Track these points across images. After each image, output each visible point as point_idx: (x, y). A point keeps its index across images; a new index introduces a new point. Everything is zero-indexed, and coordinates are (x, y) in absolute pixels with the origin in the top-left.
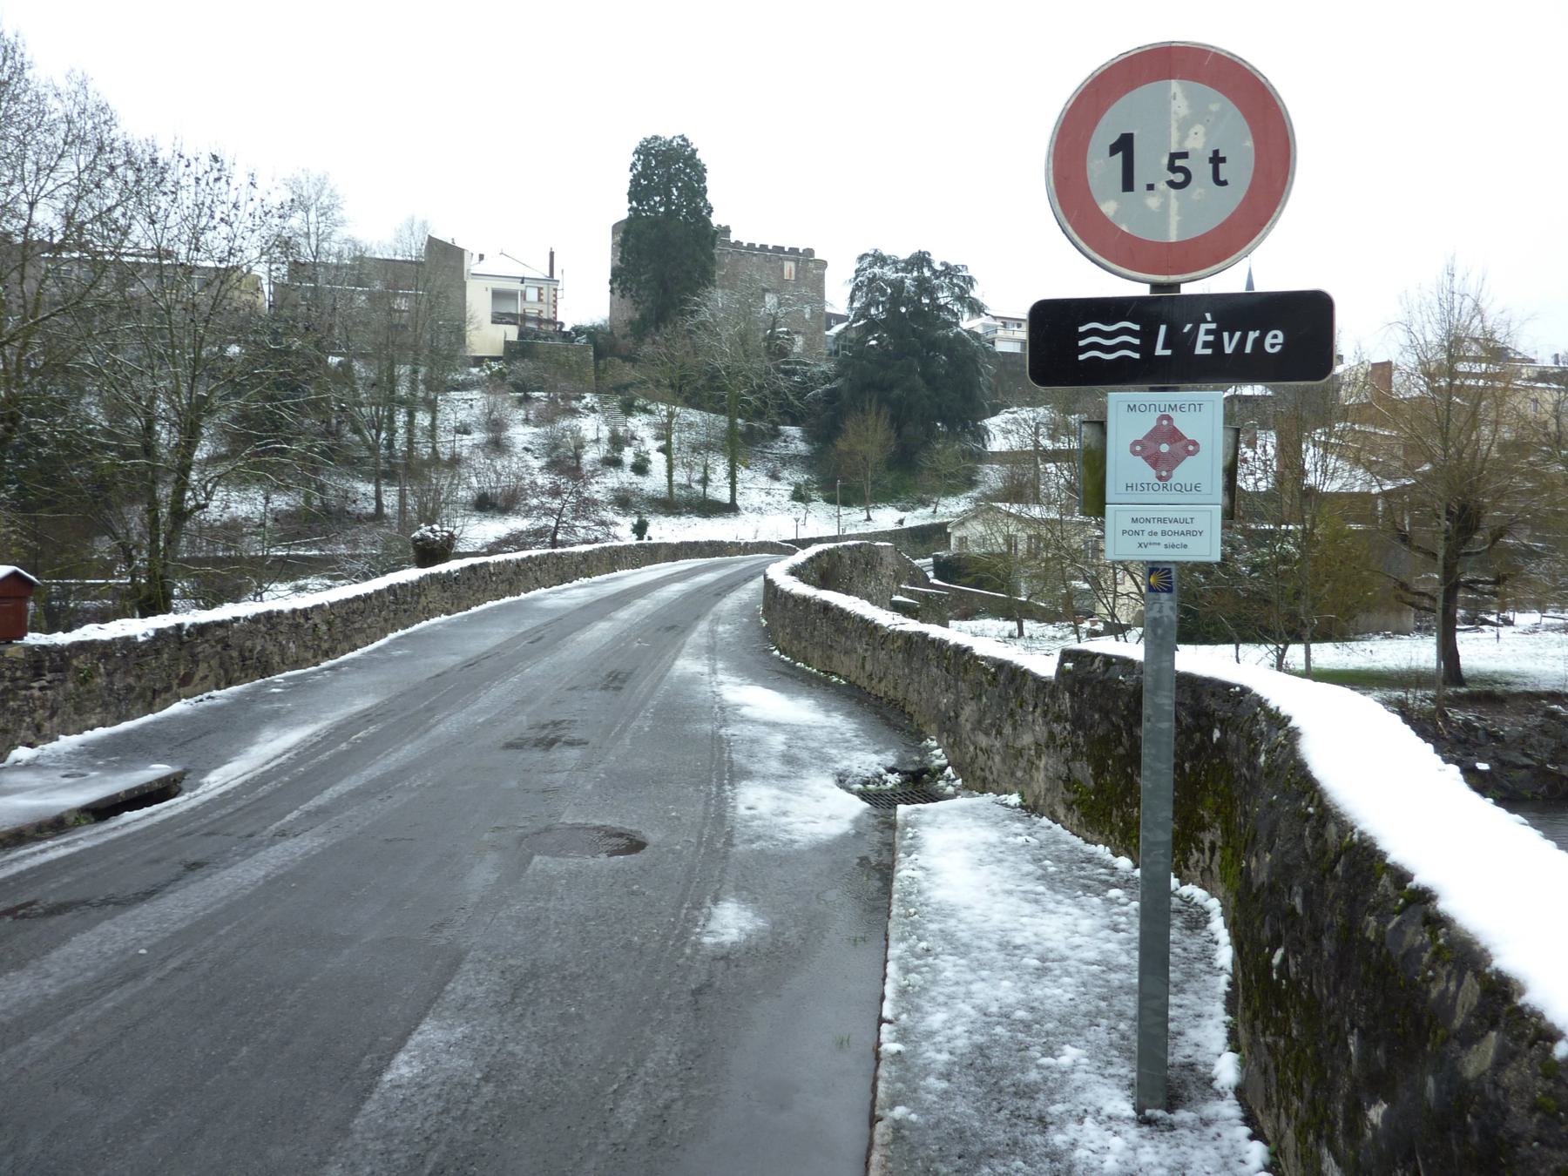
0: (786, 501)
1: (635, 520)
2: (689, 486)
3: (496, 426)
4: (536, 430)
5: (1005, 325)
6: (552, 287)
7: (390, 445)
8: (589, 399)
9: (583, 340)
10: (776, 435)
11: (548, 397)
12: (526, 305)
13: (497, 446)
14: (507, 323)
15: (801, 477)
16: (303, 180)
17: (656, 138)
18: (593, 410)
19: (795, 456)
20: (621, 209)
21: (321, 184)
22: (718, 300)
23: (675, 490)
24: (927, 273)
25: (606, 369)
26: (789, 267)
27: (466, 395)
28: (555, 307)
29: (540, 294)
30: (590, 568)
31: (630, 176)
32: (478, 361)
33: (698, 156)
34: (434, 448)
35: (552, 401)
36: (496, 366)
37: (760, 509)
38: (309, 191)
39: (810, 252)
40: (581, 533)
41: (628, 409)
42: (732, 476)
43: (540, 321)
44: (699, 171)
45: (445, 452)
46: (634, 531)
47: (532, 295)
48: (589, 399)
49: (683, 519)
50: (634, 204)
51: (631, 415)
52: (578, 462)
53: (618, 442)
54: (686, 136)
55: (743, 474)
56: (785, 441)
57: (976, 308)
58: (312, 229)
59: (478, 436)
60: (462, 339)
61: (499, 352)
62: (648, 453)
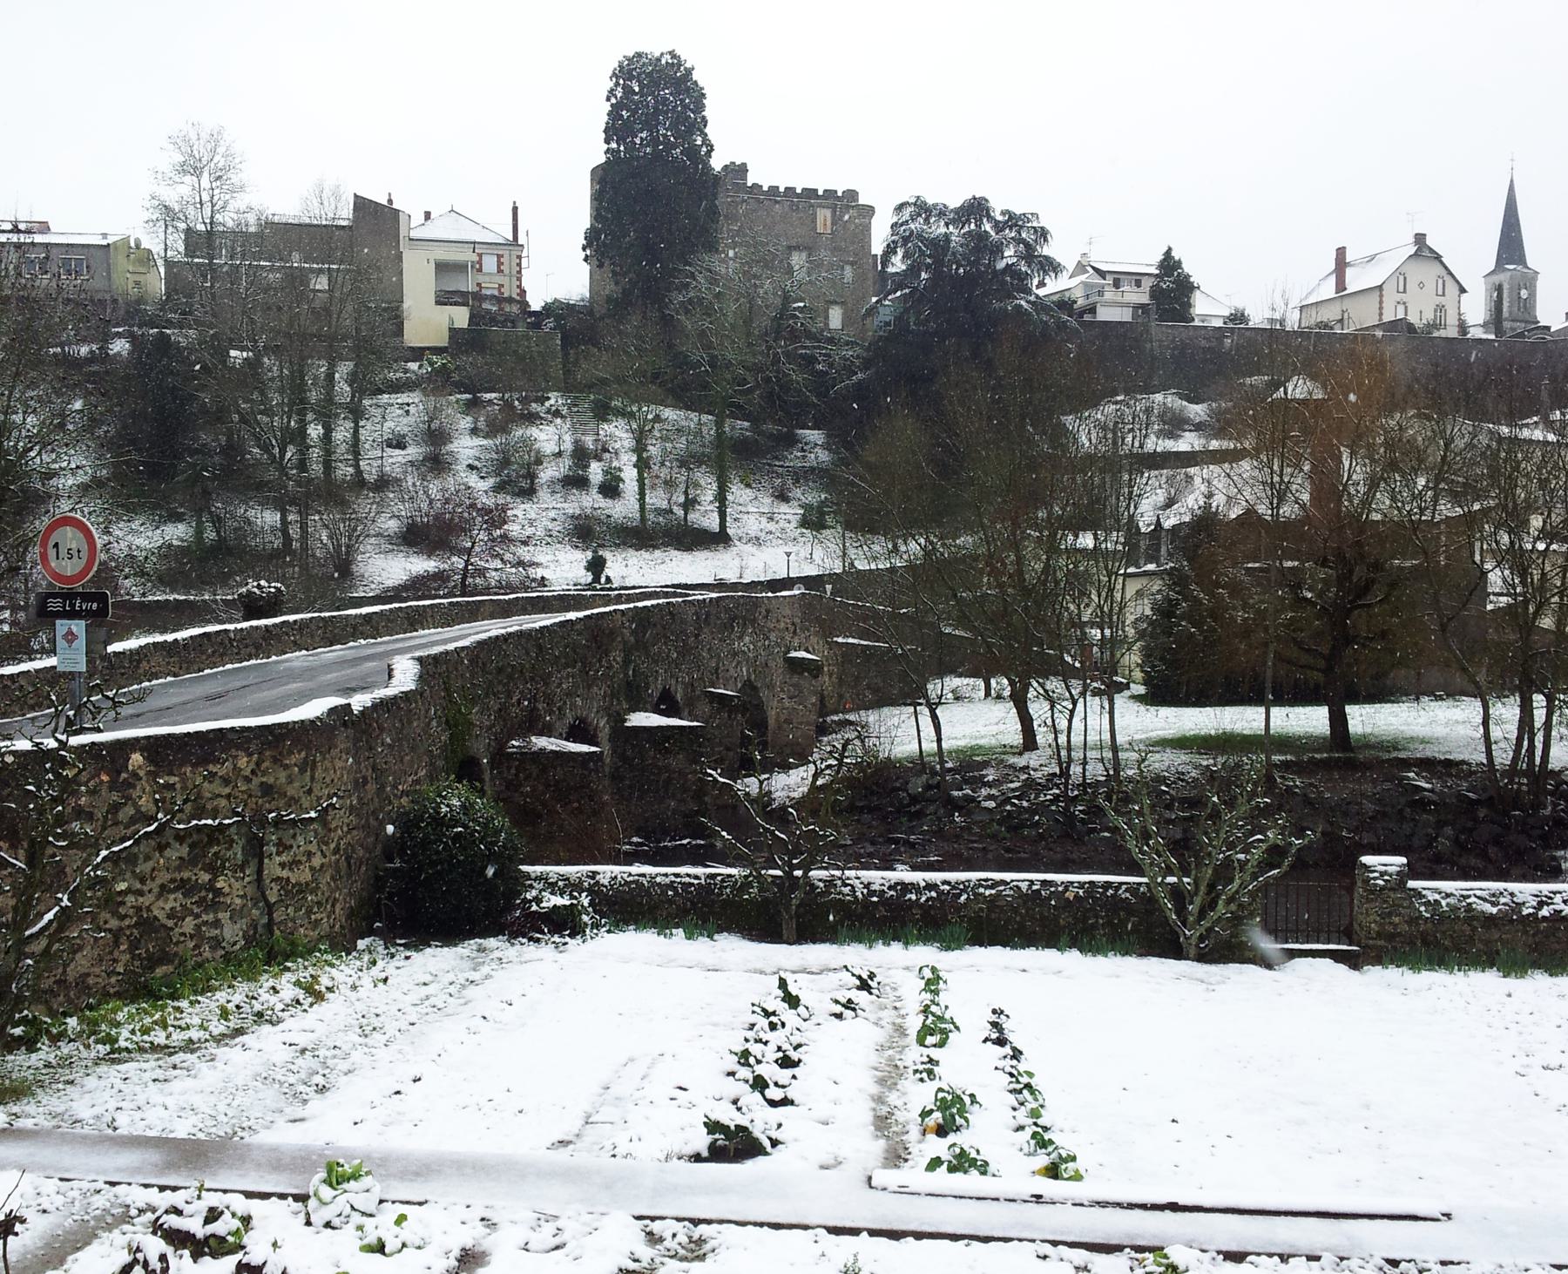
0: (792, 528)
1: (589, 554)
2: (671, 511)
3: (436, 437)
4: (485, 442)
5: (1117, 284)
6: (515, 253)
7: (302, 465)
8: (555, 399)
9: (549, 324)
10: (791, 441)
11: (502, 399)
12: (480, 279)
13: (436, 463)
14: (456, 304)
15: (813, 497)
16: (194, 137)
17: (639, 55)
18: (557, 414)
19: (812, 469)
20: (596, 152)
21: (215, 139)
22: (728, 260)
23: (647, 515)
24: (987, 227)
25: (577, 360)
26: (823, 216)
27: (403, 398)
28: (519, 279)
29: (500, 264)
30: (661, 610)
31: (607, 107)
32: (418, 354)
33: (695, 76)
34: (357, 466)
35: (508, 406)
36: (439, 361)
37: (758, 539)
38: (201, 150)
39: (852, 195)
40: (493, 576)
41: (602, 412)
42: (721, 498)
43: (499, 300)
44: (697, 98)
45: (370, 471)
46: (588, 569)
47: (490, 264)
48: (555, 399)
49: (657, 553)
50: (614, 145)
51: (606, 420)
52: (532, 483)
53: (581, 456)
54: (678, 52)
55: (739, 494)
56: (803, 450)
57: (1050, 266)
58: (206, 197)
59: (413, 452)
60: (399, 331)
61: (443, 341)
62: (620, 470)
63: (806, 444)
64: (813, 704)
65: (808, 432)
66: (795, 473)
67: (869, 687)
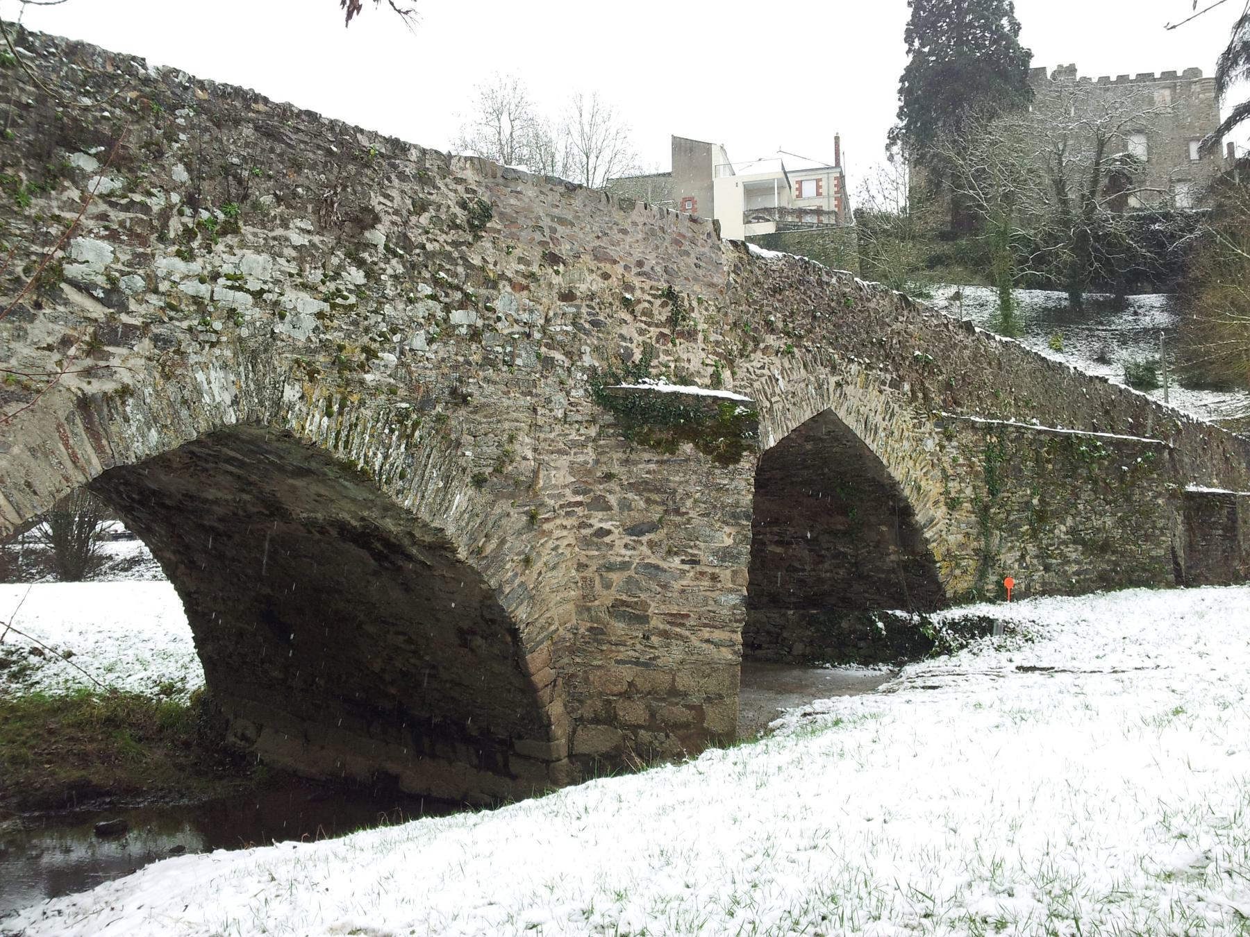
10: (1119, 306)
19: (1146, 330)
29: (818, 187)
56: (1136, 313)
63: (1140, 307)
64: (725, 555)
65: (1142, 296)
66: (1122, 334)
67: (1075, 536)
